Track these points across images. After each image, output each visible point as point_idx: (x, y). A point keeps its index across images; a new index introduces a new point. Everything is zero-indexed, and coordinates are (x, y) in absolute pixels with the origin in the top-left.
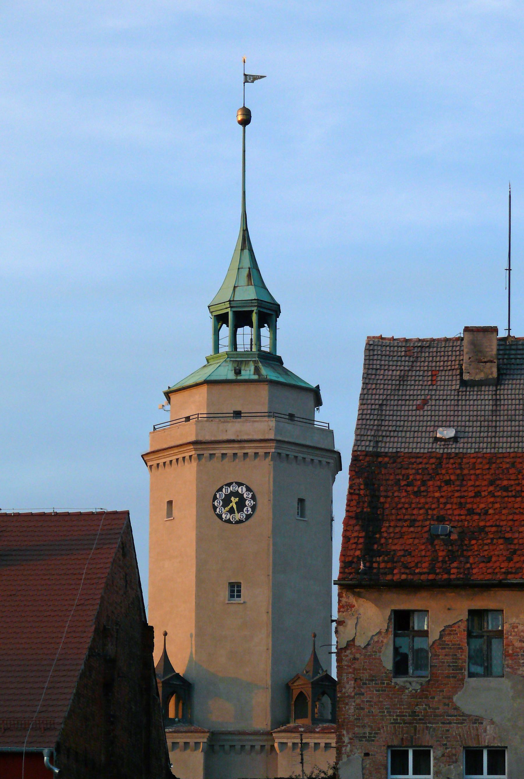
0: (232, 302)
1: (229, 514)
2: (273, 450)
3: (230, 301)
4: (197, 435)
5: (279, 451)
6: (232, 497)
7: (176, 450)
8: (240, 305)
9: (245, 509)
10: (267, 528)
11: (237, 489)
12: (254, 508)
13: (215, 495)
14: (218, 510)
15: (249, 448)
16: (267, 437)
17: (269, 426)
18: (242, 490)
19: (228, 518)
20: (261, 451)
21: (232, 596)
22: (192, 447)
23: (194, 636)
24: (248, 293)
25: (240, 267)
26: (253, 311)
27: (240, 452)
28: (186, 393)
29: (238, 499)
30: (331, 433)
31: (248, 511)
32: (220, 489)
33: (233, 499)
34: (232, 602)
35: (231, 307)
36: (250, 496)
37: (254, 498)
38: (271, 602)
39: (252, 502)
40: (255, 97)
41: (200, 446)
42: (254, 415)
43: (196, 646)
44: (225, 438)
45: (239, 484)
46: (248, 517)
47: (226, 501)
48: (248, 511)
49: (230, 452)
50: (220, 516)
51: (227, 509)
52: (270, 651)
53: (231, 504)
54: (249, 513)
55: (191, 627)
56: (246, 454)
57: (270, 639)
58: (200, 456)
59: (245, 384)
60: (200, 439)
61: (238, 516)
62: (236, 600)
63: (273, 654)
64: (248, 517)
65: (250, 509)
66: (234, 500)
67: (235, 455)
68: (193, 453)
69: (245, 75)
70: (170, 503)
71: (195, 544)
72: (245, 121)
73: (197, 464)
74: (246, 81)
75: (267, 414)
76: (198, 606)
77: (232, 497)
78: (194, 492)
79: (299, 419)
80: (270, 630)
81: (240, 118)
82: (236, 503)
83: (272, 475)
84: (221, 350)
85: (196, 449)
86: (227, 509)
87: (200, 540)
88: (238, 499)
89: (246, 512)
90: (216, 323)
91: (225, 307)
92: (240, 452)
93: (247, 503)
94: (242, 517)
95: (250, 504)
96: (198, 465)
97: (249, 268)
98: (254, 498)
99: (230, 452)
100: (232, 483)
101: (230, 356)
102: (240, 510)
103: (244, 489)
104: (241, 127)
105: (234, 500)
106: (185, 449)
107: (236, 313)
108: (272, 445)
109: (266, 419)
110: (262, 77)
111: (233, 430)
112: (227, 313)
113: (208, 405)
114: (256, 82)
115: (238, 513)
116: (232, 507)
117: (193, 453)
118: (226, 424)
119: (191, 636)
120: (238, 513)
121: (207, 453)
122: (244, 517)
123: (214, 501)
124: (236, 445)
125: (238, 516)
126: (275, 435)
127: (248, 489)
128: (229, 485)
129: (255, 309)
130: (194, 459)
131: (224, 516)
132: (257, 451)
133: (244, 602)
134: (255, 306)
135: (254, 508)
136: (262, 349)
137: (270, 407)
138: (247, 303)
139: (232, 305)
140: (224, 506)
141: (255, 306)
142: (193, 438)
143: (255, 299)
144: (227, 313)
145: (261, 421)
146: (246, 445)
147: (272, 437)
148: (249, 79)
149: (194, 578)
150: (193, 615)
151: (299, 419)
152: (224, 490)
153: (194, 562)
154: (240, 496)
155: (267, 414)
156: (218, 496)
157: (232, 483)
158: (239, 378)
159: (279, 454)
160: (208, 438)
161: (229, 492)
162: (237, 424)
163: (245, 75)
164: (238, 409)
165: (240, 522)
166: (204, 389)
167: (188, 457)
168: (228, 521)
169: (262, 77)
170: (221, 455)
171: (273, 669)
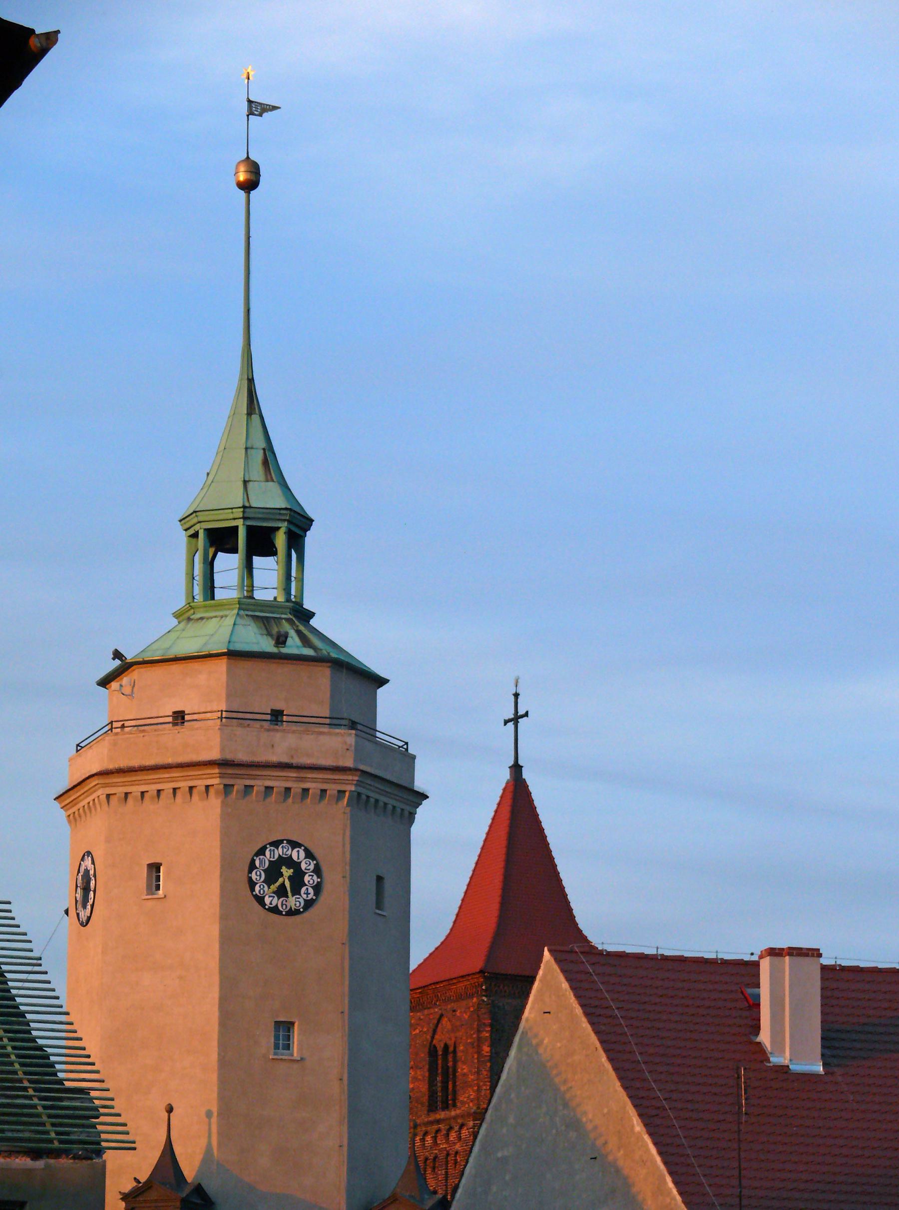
0: (247, 510)
1: (276, 898)
2: (353, 788)
3: (244, 507)
4: (222, 750)
5: (360, 790)
6: (284, 867)
7: (175, 774)
8: (260, 516)
9: (303, 890)
10: (340, 927)
11: (289, 852)
12: (317, 889)
13: (253, 861)
14: (257, 888)
15: (314, 780)
16: (342, 763)
17: (345, 743)
18: (297, 855)
19: (274, 903)
20: (333, 789)
21: (276, 1047)
22: (217, 771)
23: (215, 1114)
24: (268, 497)
25: (249, 445)
26: (278, 528)
27: (296, 787)
28: (175, 668)
29: (292, 870)
30: (409, 760)
31: (308, 894)
32: (261, 852)
33: (284, 870)
34: (281, 1057)
35: (244, 518)
36: (312, 867)
37: (317, 871)
38: (346, 1062)
39: (315, 877)
40: (267, 143)
41: (230, 771)
42: (306, 723)
43: (220, 1134)
44: (274, 759)
45: (294, 844)
46: (309, 904)
47: (273, 873)
48: (308, 894)
49: (279, 785)
50: (260, 900)
51: (274, 887)
52: (345, 1149)
53: (281, 880)
54: (310, 897)
55: (210, 1098)
56: (306, 791)
57: (345, 1128)
58: (228, 788)
59: (306, 663)
60: (229, 757)
61: (293, 902)
62: (284, 1055)
63: (349, 1155)
64: (309, 904)
65: (311, 891)
66: (287, 872)
67: (288, 790)
68: (216, 781)
69: (250, 102)
70: (155, 868)
71: (217, 946)
72: (249, 186)
73: (223, 802)
74: (251, 113)
75: (328, 721)
76: (223, 1063)
77: (284, 867)
78: (217, 852)
79: (290, 719)
80: (345, 1111)
81: (242, 177)
82: (290, 878)
83: (348, 833)
84: (219, 594)
85: (222, 776)
86: (274, 887)
87: (226, 939)
88: (292, 870)
89: (305, 896)
90: (208, 544)
91: (231, 516)
92: (296, 787)
93: (307, 878)
94: (298, 904)
95: (311, 882)
96: (224, 804)
97: (264, 449)
98: (317, 871)
99: (279, 785)
100: (281, 842)
101: (244, 606)
102: (296, 891)
103: (302, 854)
104: (242, 194)
105: (287, 872)
106: (200, 773)
107: (250, 530)
108: (350, 778)
109: (325, 729)
110: (275, 108)
111: (282, 745)
112: (236, 528)
113: (229, 696)
114: (265, 114)
115: (293, 896)
116: (283, 884)
117: (216, 781)
118: (272, 733)
119: (209, 1114)
120: (293, 896)
121: (239, 784)
122: (302, 904)
123: (250, 872)
124: (293, 774)
125: (293, 902)
126: (355, 760)
127: (309, 855)
128: (276, 844)
129: (284, 526)
130: (217, 793)
131: (267, 900)
132: (325, 786)
133: (302, 1059)
134: (285, 520)
135: (317, 889)
136: (259, 595)
137: (332, 709)
138: (273, 514)
139: (246, 515)
140: (269, 881)
141: (285, 520)
142: (214, 754)
143: (286, 509)
144: (236, 528)
145: (329, 734)
146: (309, 775)
147: (349, 763)
148: (256, 109)
149: (216, 1009)
150: (214, 1077)
151: (290, 719)
152: (267, 853)
153: (216, 979)
154: (289, 862)
155: (328, 721)
156: (257, 863)
157: (281, 842)
158: (284, 650)
159: (359, 794)
160: (242, 756)
161: (276, 856)
162: (290, 735)
163: (250, 102)
164: (278, 706)
165: (292, 913)
166: (222, 665)
167: (203, 788)
168: (275, 910)
169: (275, 108)
170: (263, 789)
171: (348, 1182)
